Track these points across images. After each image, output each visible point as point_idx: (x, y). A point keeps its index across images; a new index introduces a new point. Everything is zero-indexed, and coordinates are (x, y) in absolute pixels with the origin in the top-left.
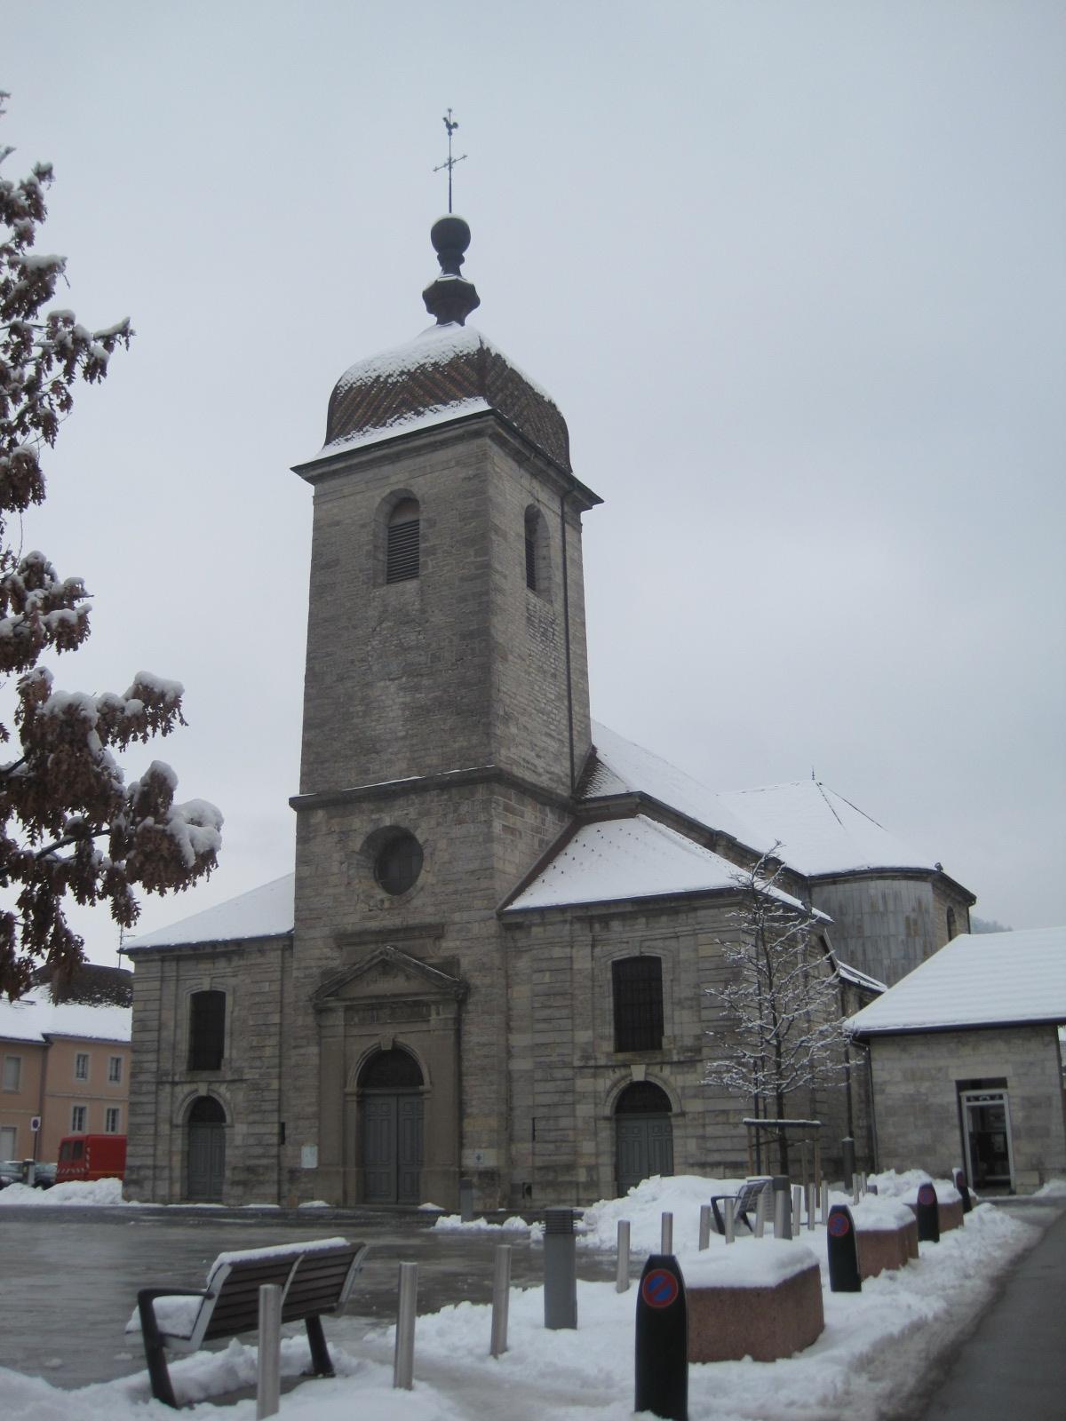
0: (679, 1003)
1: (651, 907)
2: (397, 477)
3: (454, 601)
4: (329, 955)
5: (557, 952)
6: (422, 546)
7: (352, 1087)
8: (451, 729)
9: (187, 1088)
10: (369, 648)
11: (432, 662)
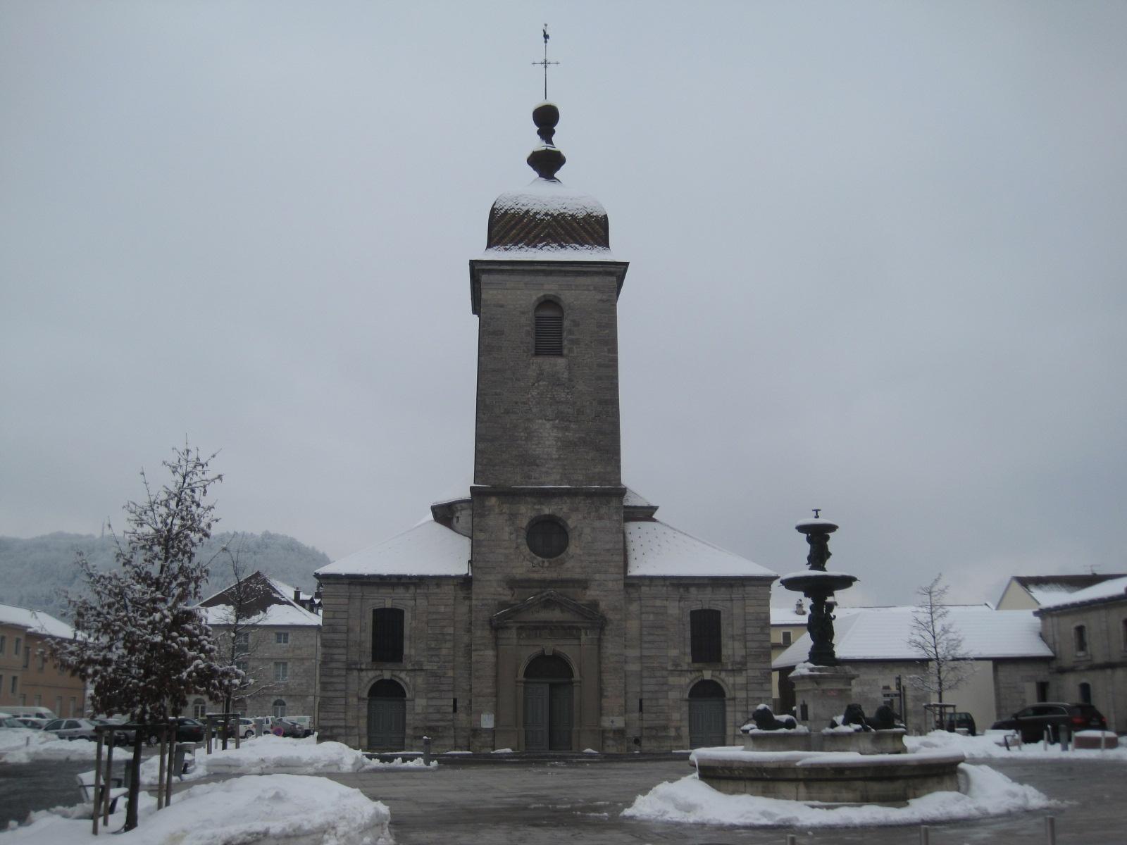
2: (550, 286)
3: (593, 378)
4: (501, 592)
5: (658, 603)
7: (521, 677)
9: (371, 674)
10: (530, 396)
11: (578, 414)
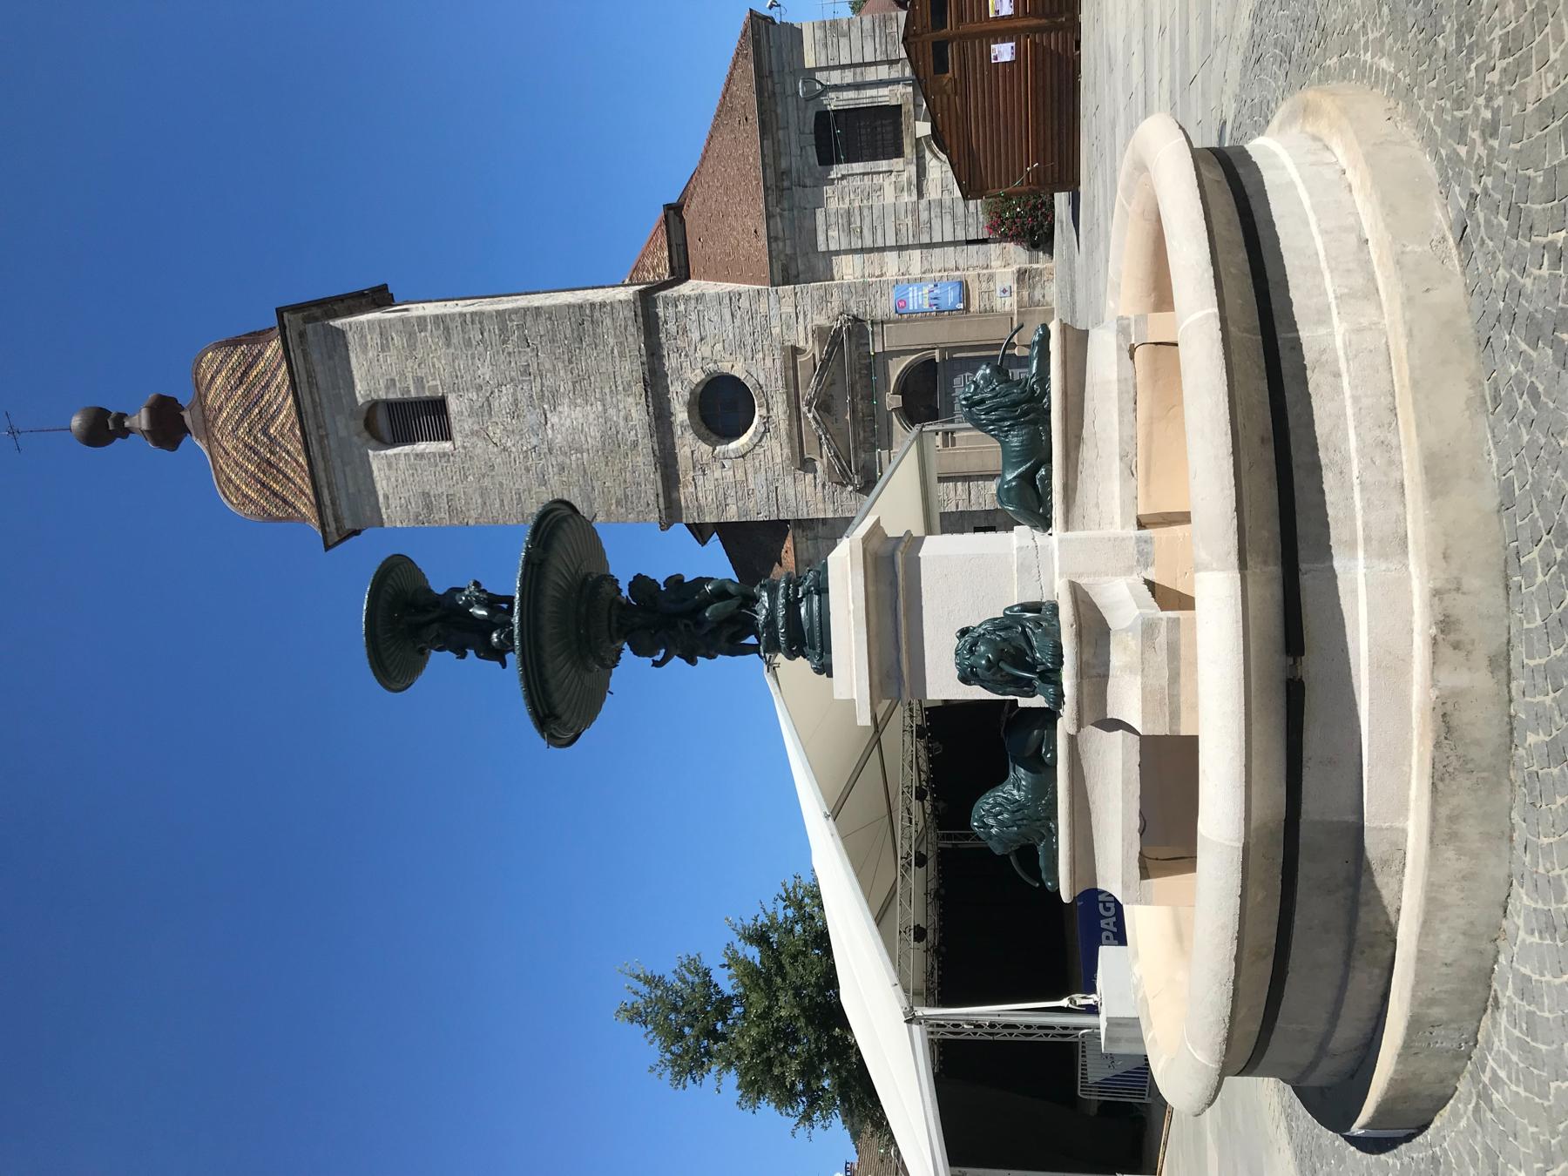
6: (413, 394)
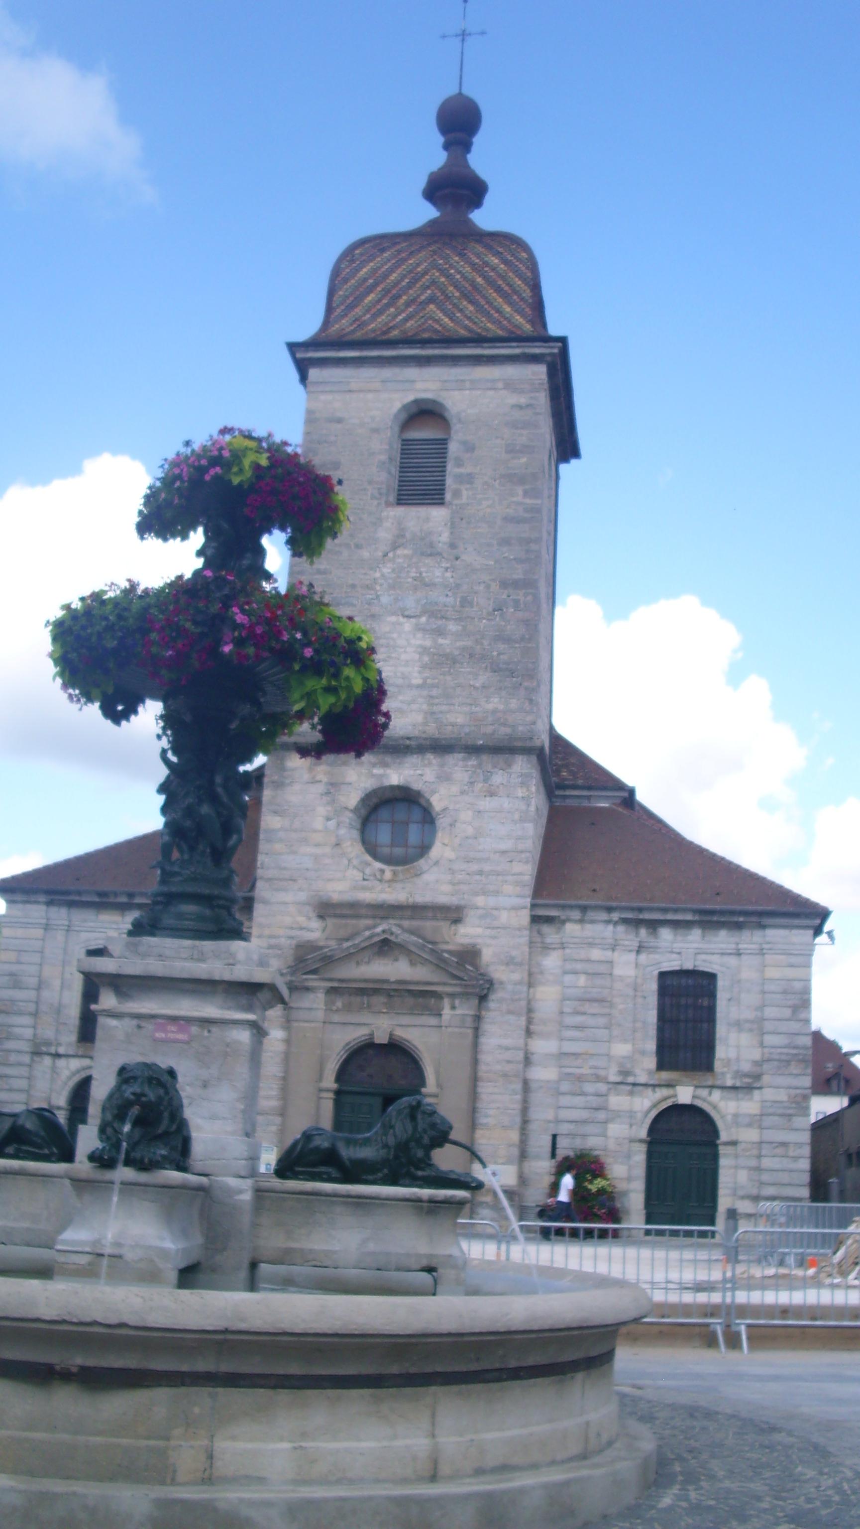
0: (738, 1025)
1: (715, 918)
3: (495, 542)
4: (304, 925)
7: (329, 1082)
8: (483, 687)
9: (75, 1064)
10: (378, 575)
